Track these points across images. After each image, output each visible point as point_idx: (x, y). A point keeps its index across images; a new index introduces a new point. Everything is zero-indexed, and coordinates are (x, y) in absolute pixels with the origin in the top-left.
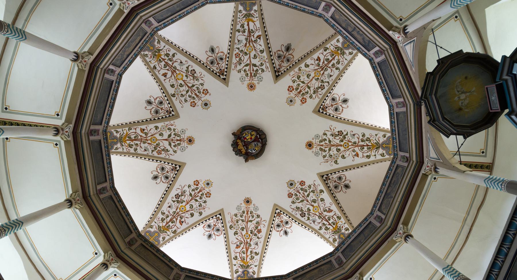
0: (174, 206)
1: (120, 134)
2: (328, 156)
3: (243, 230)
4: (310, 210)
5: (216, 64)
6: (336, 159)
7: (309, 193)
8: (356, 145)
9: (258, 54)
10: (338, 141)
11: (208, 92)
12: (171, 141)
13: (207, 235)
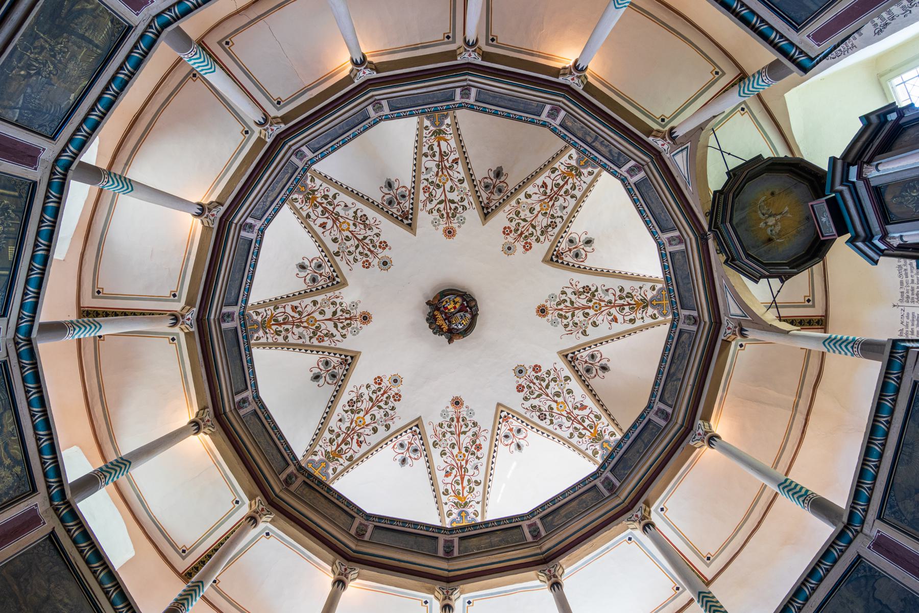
0: (346, 418)
1: (263, 316)
2: (571, 324)
3: (453, 448)
4: (552, 409)
5: (396, 203)
6: (584, 329)
7: (549, 382)
10: (584, 302)
11: (387, 246)
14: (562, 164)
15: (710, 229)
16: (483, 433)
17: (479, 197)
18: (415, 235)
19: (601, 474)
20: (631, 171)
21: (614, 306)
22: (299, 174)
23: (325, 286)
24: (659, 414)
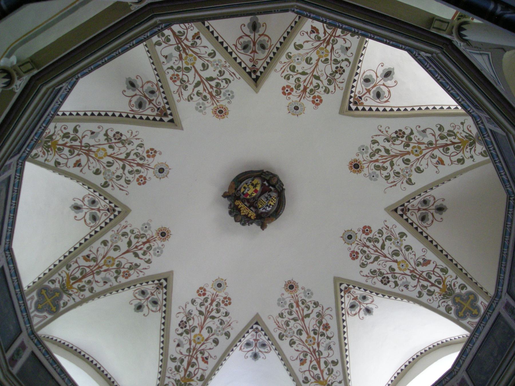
0: (184, 340)
1: (59, 281)
2: (392, 175)
3: (301, 334)
4: (393, 270)
5: (148, 103)
6: (408, 177)
7: (384, 242)
8: (434, 146)
9: (208, 61)
10: (401, 148)
11: (155, 152)
12: (136, 249)
13: (251, 356)
16: (328, 312)
18: (182, 129)
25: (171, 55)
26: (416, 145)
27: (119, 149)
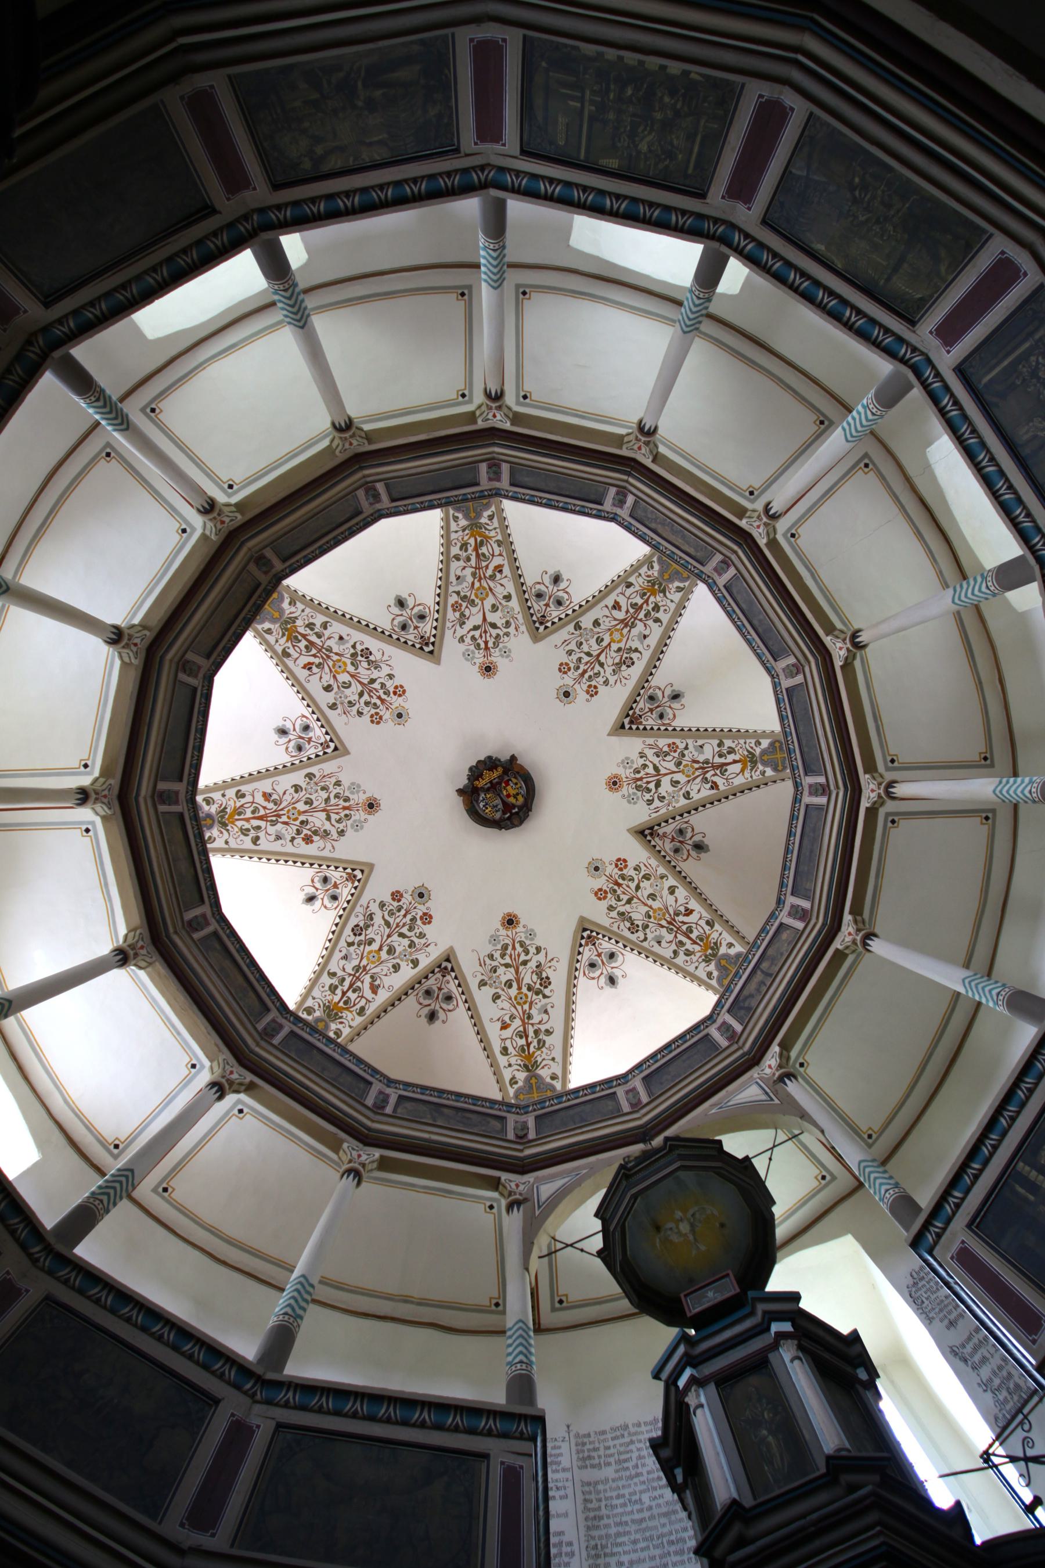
0: (344, 647)
1: (488, 525)
3: (306, 803)
4: (370, 944)
5: (651, 707)
7: (408, 937)
11: (592, 696)
14: (720, 934)
15: (667, 1139)
16: (329, 846)
17: (666, 821)
18: (609, 735)
19: (286, 1018)
20: (725, 1028)
21: (524, 1024)
22: (695, 567)
23: (532, 611)
24: (381, 1096)
25: (703, 753)
26: (529, 1000)
27: (613, 658)
